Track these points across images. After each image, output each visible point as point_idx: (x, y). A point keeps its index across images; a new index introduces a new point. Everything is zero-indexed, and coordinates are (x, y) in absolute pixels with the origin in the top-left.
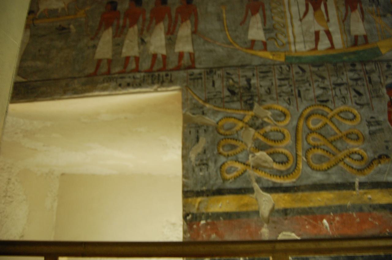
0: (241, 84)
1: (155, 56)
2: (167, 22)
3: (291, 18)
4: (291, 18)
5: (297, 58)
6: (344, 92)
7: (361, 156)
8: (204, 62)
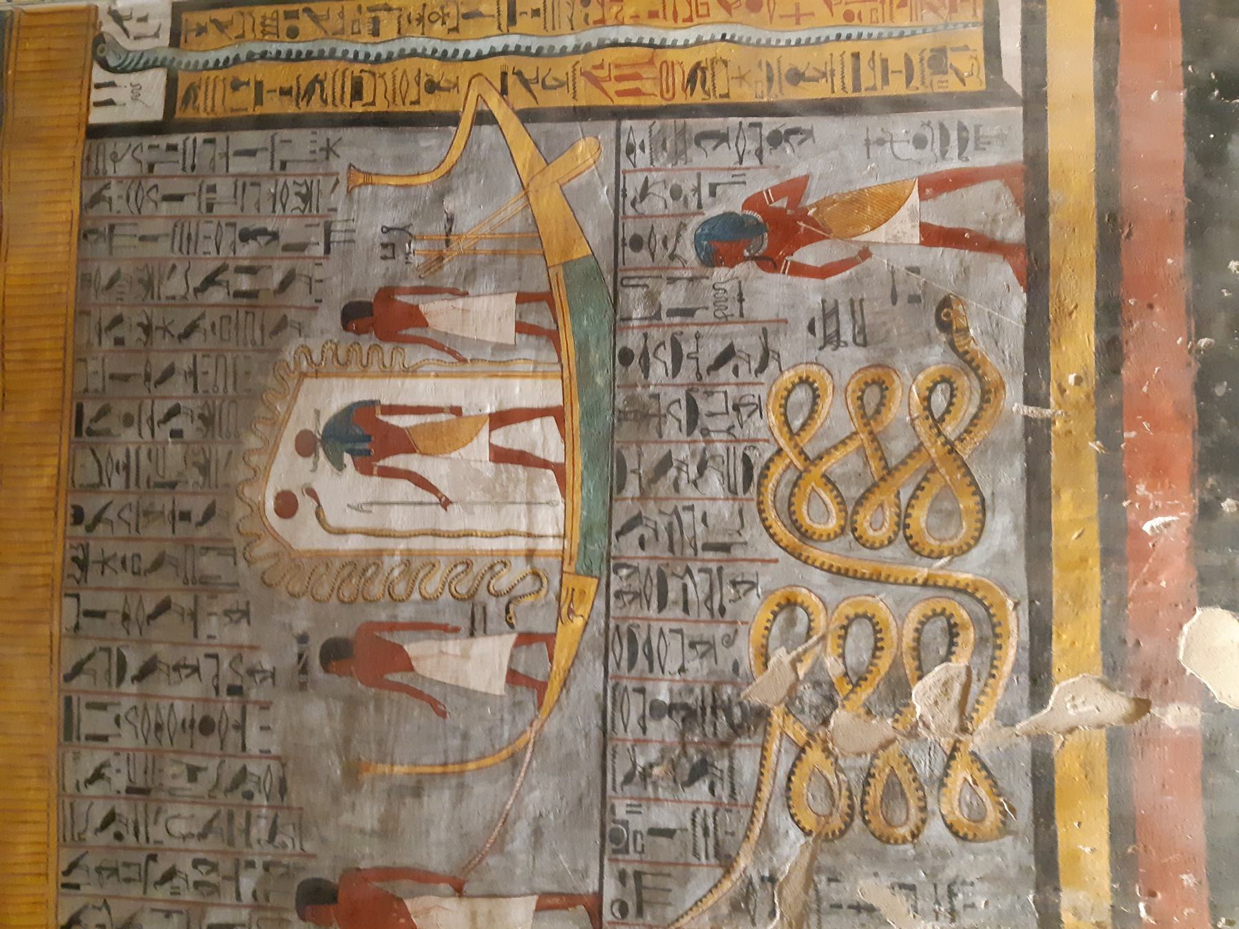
3: (436, 534)
4: (436, 534)
5: (587, 535)
6: (718, 403)
7: (936, 384)
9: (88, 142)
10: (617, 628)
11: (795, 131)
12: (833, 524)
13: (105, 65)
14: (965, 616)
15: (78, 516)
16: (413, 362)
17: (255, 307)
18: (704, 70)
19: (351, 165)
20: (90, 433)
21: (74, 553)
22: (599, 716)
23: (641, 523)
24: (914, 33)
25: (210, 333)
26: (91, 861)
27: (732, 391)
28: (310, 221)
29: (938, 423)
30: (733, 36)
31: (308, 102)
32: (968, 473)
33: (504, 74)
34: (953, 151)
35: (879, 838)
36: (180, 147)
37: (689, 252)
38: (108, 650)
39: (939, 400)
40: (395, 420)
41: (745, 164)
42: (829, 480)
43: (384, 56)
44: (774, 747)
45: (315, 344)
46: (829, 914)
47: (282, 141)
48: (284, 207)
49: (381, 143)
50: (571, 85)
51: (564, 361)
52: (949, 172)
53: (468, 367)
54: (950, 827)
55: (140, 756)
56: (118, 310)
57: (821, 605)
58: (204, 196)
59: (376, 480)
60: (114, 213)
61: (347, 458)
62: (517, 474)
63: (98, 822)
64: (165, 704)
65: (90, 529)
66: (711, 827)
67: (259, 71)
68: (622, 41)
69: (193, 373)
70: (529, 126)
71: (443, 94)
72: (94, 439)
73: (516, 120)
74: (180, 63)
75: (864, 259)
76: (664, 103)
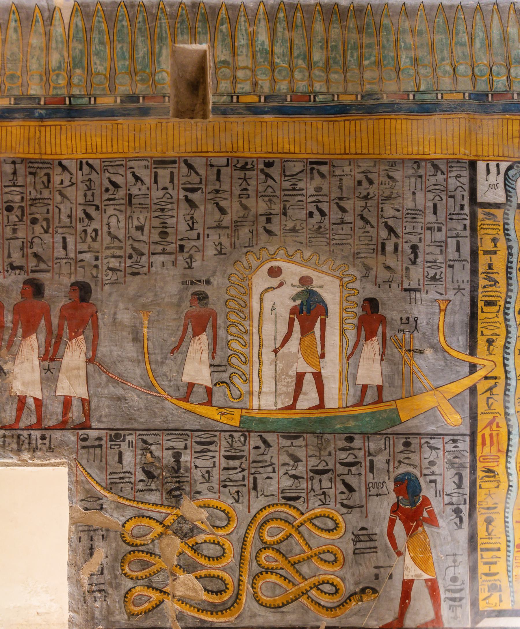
0: (165, 462)
1: (22, 401)
2: (42, 337)
3: (260, 347)
4: (260, 347)
5: (261, 421)
6: (326, 484)
7: (335, 586)
8: (104, 414)
9: (467, 161)
10: (215, 436)
11: (461, 521)
12: (267, 539)
13: (510, 168)
14: (225, 599)
15: (269, 164)
16: (347, 334)
17: (377, 254)
18: (494, 476)
19: (450, 301)
20: (312, 169)
21: (250, 163)
22: (174, 428)
23: (266, 447)
24: (509, 577)
25: (363, 230)
26: (94, 176)
27: (332, 492)
28: (421, 281)
29: (316, 587)
30: (511, 491)
31: (484, 278)
32: (293, 601)
33: (495, 378)
34: (449, 595)
35: (123, 558)
36: (462, 212)
37: (403, 469)
38: (201, 183)
39: (327, 588)
40: (318, 325)
41: (445, 497)
42: (288, 537)
43: (507, 317)
44: (162, 510)
45: (357, 285)
46: (88, 535)
47: (464, 265)
48: (429, 267)
49: (461, 316)
50: (490, 411)
51: (347, 409)
52: (439, 594)
53: (345, 361)
54: (130, 590)
55: (148, 201)
56: (376, 182)
57: (228, 532)
58: (436, 225)
59: (288, 316)
60: (428, 177)
61: (298, 302)
62: (291, 386)
63: (113, 179)
64: (174, 213)
65: (262, 171)
66: (124, 481)
67: (502, 253)
68: (511, 436)
69: (342, 222)
70: (468, 391)
71: (486, 348)
72: (308, 171)
73: (471, 384)
74: (508, 210)
75: (397, 553)
76: (478, 458)
